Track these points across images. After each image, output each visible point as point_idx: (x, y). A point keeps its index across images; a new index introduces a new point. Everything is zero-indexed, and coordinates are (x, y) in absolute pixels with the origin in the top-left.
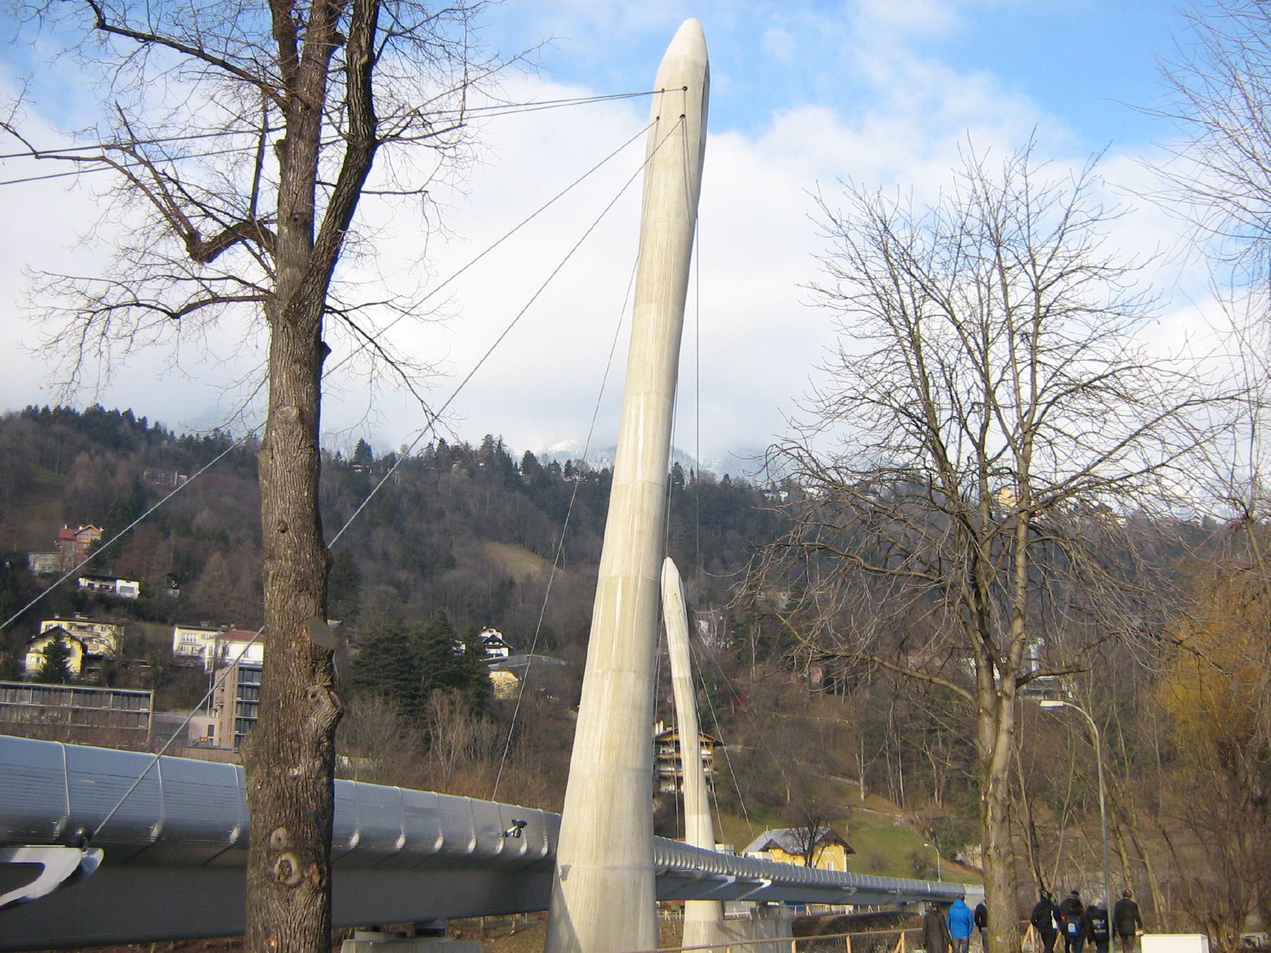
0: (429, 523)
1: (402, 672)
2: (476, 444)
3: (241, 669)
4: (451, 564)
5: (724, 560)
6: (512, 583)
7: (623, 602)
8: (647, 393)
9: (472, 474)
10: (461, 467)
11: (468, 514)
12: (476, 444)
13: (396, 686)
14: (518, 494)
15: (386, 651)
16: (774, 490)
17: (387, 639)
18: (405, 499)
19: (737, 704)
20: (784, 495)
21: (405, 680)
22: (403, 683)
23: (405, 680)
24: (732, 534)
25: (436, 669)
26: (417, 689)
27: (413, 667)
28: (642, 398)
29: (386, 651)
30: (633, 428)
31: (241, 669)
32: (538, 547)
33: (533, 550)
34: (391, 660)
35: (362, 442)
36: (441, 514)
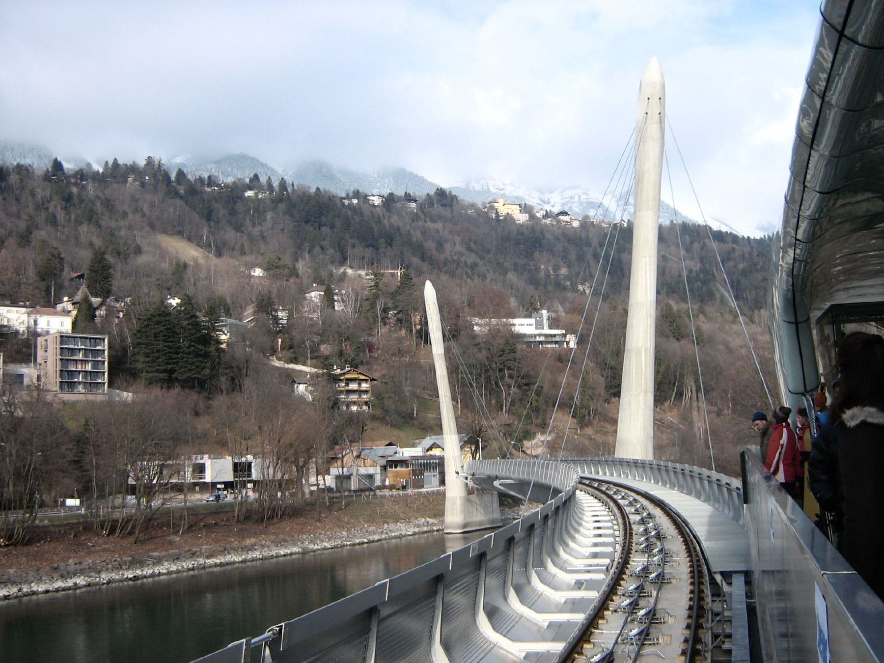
0: (117, 221)
1: (169, 337)
2: (142, 163)
3: (62, 337)
4: (138, 251)
5: (322, 248)
6: (185, 266)
7: (646, 355)
8: (650, 257)
9: (143, 185)
10: (135, 180)
11: (144, 215)
12: (142, 163)
13: (166, 346)
14: (178, 202)
15: (158, 323)
16: (348, 197)
17: (160, 315)
18: (98, 204)
19: (370, 351)
20: (355, 201)
21: (172, 342)
22: (170, 344)
23: (172, 342)
24: (325, 230)
25: (192, 334)
26: (179, 347)
27: (175, 333)
28: (648, 259)
29: (158, 323)
30: (644, 274)
31: (62, 337)
32: (193, 238)
33: (189, 239)
34: (162, 328)
35: (56, 160)
36: (125, 215)
